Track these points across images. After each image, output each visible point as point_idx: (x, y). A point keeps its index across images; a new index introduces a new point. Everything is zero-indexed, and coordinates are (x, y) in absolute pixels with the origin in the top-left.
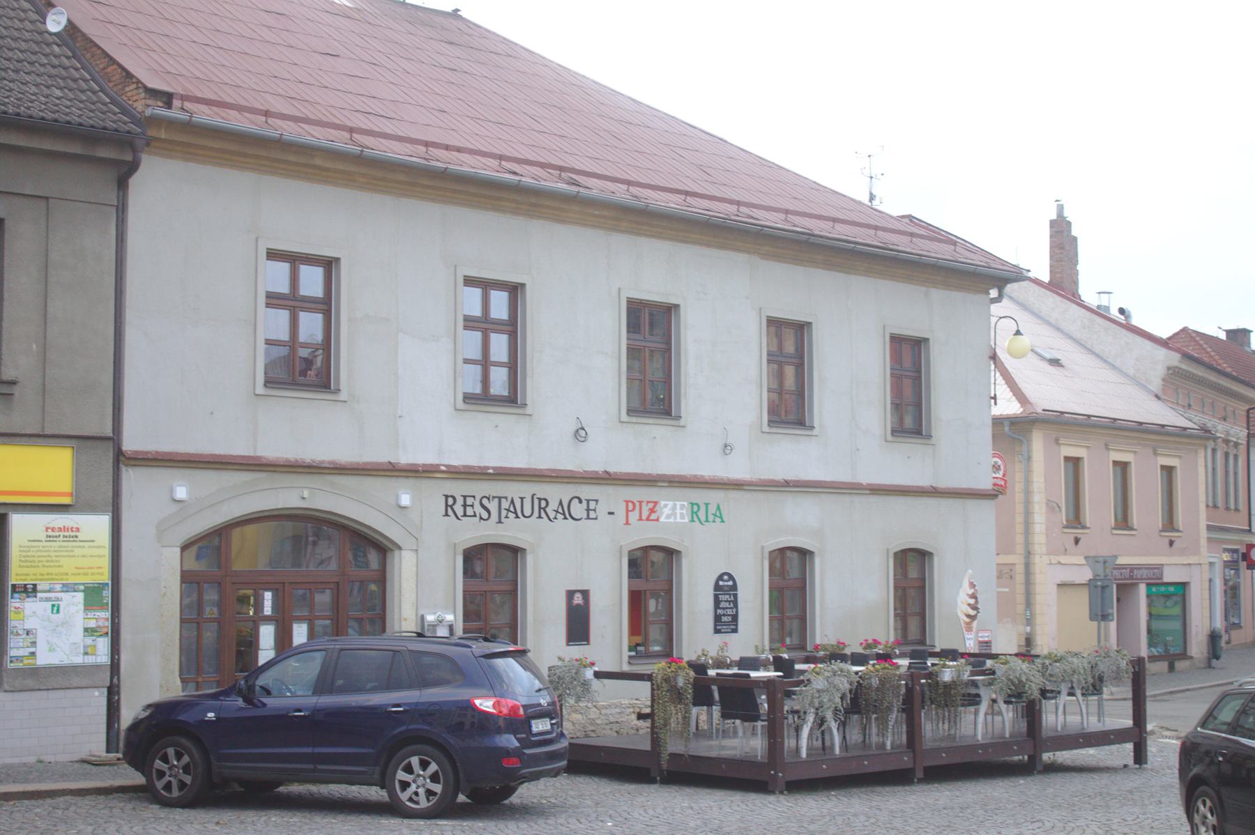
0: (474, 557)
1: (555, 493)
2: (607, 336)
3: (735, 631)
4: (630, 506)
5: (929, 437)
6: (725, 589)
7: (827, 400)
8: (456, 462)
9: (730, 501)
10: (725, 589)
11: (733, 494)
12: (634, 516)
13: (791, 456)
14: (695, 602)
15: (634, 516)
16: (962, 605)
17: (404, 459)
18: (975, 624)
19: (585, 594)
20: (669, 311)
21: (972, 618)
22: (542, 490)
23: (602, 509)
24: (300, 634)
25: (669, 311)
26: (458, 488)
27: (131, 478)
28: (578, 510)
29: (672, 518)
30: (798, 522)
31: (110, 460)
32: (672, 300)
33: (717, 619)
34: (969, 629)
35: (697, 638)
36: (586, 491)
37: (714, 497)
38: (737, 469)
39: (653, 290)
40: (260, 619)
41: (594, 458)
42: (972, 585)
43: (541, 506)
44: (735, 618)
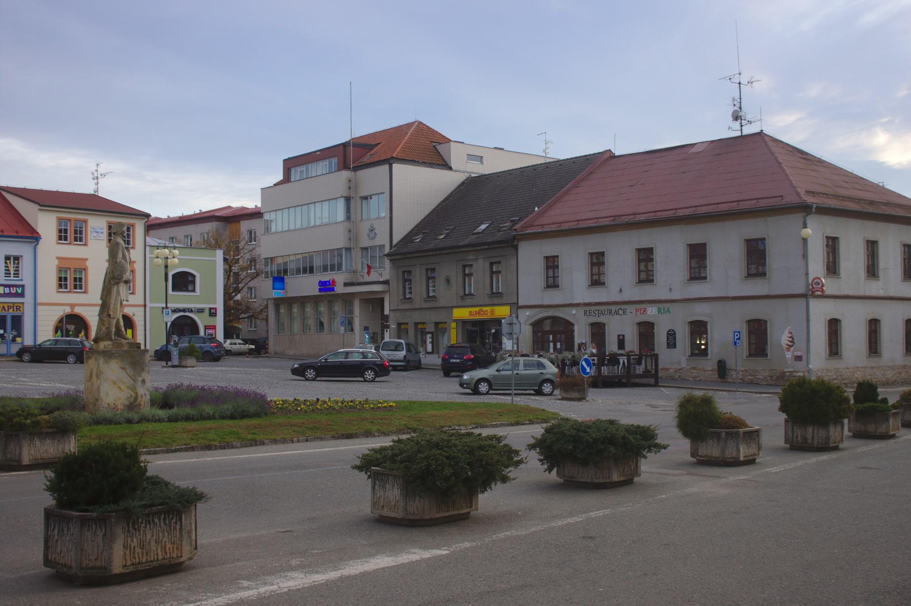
0: (593, 325)
1: (614, 308)
2: (539, 266)
3: (675, 347)
4: (637, 310)
5: (839, 274)
6: (671, 335)
7: (845, 265)
8: (587, 301)
9: (673, 307)
10: (671, 335)
11: (674, 304)
12: (638, 313)
13: (874, 288)
14: (661, 338)
15: (638, 313)
16: (785, 340)
17: (575, 302)
18: (792, 349)
19: (623, 336)
20: (703, 246)
21: (791, 346)
22: (610, 307)
23: (628, 312)
24: (558, 346)
25: (703, 246)
26: (587, 308)
27: (520, 311)
28: (621, 312)
29: (651, 312)
30: (700, 312)
31: (516, 307)
32: (651, 246)
33: (668, 344)
34: (788, 350)
35: (612, 346)
36: (623, 307)
37: (666, 306)
38: (676, 295)
39: (645, 244)
40: (549, 342)
41: (626, 297)
42: (790, 333)
43: (610, 312)
44: (675, 344)
